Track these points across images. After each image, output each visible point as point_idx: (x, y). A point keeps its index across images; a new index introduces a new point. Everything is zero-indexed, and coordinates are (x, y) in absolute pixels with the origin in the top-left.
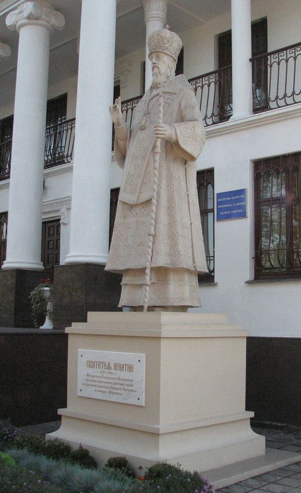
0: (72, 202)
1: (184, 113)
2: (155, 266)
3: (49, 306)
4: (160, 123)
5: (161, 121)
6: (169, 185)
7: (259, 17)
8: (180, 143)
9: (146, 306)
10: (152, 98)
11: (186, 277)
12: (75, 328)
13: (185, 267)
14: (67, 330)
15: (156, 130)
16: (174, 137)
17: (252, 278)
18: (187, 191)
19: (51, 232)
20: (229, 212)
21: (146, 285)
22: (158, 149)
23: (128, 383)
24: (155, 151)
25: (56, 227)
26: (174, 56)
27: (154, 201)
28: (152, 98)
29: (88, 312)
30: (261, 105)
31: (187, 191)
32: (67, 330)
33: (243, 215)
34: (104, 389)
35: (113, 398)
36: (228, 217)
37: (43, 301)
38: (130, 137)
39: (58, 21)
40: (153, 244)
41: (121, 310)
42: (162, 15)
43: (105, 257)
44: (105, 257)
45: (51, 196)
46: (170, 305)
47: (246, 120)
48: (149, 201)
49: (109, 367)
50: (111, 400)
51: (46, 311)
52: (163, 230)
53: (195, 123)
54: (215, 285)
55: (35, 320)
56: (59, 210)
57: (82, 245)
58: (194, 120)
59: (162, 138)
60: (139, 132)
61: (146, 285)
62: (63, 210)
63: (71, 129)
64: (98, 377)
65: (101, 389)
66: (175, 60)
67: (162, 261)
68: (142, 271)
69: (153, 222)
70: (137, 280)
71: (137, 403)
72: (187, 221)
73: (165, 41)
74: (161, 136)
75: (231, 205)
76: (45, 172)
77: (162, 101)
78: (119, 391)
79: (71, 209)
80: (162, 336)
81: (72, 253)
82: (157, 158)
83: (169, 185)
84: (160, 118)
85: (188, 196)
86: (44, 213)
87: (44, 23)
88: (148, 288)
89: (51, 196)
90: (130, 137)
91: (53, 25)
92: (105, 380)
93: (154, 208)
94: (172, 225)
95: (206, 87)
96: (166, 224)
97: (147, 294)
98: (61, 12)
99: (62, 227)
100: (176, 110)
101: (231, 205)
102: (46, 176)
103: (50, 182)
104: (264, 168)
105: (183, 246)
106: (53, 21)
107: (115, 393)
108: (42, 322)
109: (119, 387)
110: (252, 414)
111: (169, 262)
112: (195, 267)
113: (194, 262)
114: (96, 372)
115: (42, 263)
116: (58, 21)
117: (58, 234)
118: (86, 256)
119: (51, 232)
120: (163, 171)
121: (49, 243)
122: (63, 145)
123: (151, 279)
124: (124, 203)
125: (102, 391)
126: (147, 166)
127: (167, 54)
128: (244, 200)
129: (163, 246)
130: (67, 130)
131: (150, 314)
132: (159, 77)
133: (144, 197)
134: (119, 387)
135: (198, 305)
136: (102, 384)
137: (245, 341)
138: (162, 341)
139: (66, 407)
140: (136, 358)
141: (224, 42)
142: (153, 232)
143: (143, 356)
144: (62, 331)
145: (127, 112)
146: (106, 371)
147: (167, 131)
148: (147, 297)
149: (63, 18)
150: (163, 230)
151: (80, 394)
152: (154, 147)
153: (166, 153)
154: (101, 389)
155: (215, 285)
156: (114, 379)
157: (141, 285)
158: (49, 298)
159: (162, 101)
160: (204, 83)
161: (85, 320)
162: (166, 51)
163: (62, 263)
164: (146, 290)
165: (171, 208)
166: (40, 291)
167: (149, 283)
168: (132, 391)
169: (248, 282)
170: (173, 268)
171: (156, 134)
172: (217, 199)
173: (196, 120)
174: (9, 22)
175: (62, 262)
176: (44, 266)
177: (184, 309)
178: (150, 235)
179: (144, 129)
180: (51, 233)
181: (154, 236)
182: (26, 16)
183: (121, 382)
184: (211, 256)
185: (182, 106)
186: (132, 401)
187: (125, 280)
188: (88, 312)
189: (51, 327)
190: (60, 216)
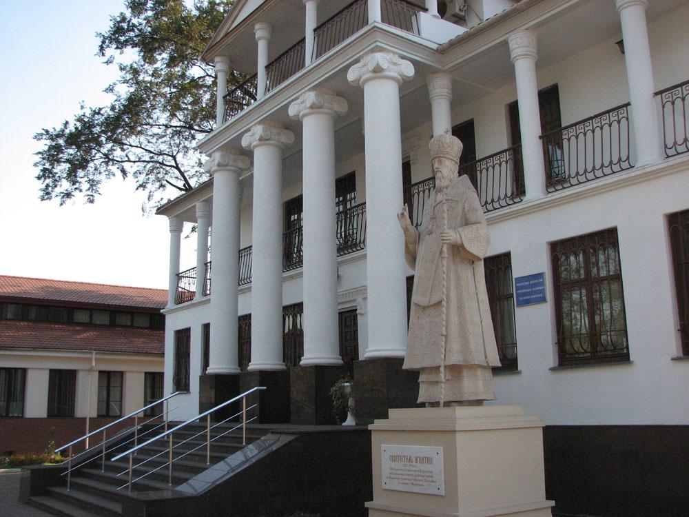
0: (369, 291)
1: (467, 216)
2: (448, 364)
3: (351, 402)
4: (445, 230)
5: (446, 227)
6: (458, 286)
7: (547, 84)
8: (465, 246)
9: (442, 402)
10: (437, 205)
11: (479, 372)
12: (378, 424)
13: (477, 363)
14: (370, 427)
15: (442, 236)
16: (459, 241)
17: (556, 364)
18: (476, 289)
19: (348, 323)
20: (529, 297)
21: (441, 382)
22: (445, 255)
23: (428, 474)
24: (442, 255)
25: (353, 333)
26: (455, 159)
27: (444, 303)
28: (437, 205)
29: (389, 410)
30: (554, 179)
31: (476, 289)
32: (370, 427)
33: (543, 300)
34: (407, 481)
35: (416, 489)
36: (528, 302)
37: (344, 397)
38: (419, 241)
39: (341, 107)
40: (445, 344)
41: (423, 405)
42: (447, 93)
43: (402, 350)
44: (402, 350)
45: (346, 286)
46: (465, 399)
47: (539, 202)
48: (440, 303)
49: (410, 460)
50: (415, 491)
51: (347, 407)
52: (454, 329)
53: (479, 225)
54: (519, 373)
55: (337, 417)
56: (355, 300)
57: (381, 338)
58: (477, 223)
59: (447, 243)
60: (427, 236)
61: (441, 382)
62: (359, 299)
63: (362, 213)
64: (401, 470)
65: (404, 481)
66: (456, 163)
67: (454, 359)
68: (438, 368)
69: (444, 323)
70: (433, 378)
71: (437, 493)
72: (477, 319)
73: (445, 146)
74: (447, 241)
75: (531, 291)
76: (339, 260)
77: (445, 208)
78: (421, 483)
79: (367, 298)
80: (457, 429)
81: (370, 348)
82: (445, 262)
83: (458, 286)
84: (444, 224)
85: (477, 294)
86: (340, 303)
87: (326, 110)
88: (442, 385)
89: (346, 286)
90: (419, 241)
91: (336, 112)
92: (408, 473)
93: (444, 310)
94: (462, 325)
95: (497, 167)
96: (457, 323)
97: (443, 391)
98: (344, 97)
99: (360, 320)
100: (460, 214)
101: (531, 291)
102: (340, 264)
103: (344, 270)
104: (559, 249)
105: (474, 343)
106: (336, 107)
107: (417, 485)
108: (345, 419)
109: (420, 478)
110: (553, 503)
111: (461, 359)
112: (487, 362)
113: (486, 358)
114: (398, 465)
115: (341, 357)
116: (341, 107)
117: (356, 325)
118: (385, 350)
119: (348, 323)
120: (452, 273)
121: (346, 321)
122: (355, 226)
123: (445, 377)
124: (417, 305)
125: (405, 484)
126: (436, 269)
127: (449, 159)
128: (543, 284)
129: (455, 345)
130: (358, 215)
131: (448, 409)
132: (443, 180)
133: (435, 299)
134: (420, 478)
135: (492, 398)
136: (405, 477)
137: (540, 432)
138: (457, 434)
139: (372, 500)
140: (434, 450)
141: (513, 111)
142: (445, 333)
143: (440, 449)
144: (365, 427)
145: (419, 195)
146: (408, 464)
147: (452, 236)
148: (443, 393)
149: (347, 104)
150: (454, 329)
151: (386, 487)
152: (441, 252)
153: (453, 256)
154: (404, 481)
155: (519, 373)
156: (415, 471)
157: (437, 382)
158: (350, 395)
159: (445, 208)
160: (495, 162)
161: (386, 416)
162: (447, 156)
163: (361, 358)
164: (441, 388)
165: (461, 308)
166: (341, 386)
167: (444, 381)
168: (433, 481)
169: (553, 369)
170: (466, 365)
171: (442, 236)
172: (516, 283)
173: (480, 223)
174: (292, 112)
175: (362, 357)
176: (342, 360)
177: (479, 402)
178: (442, 335)
179: (431, 233)
180: (348, 323)
181: (446, 336)
182: (308, 106)
183: (421, 474)
184: (508, 342)
185: (466, 209)
186: (434, 491)
187: (422, 378)
188: (389, 410)
189: (354, 424)
190: (356, 306)
